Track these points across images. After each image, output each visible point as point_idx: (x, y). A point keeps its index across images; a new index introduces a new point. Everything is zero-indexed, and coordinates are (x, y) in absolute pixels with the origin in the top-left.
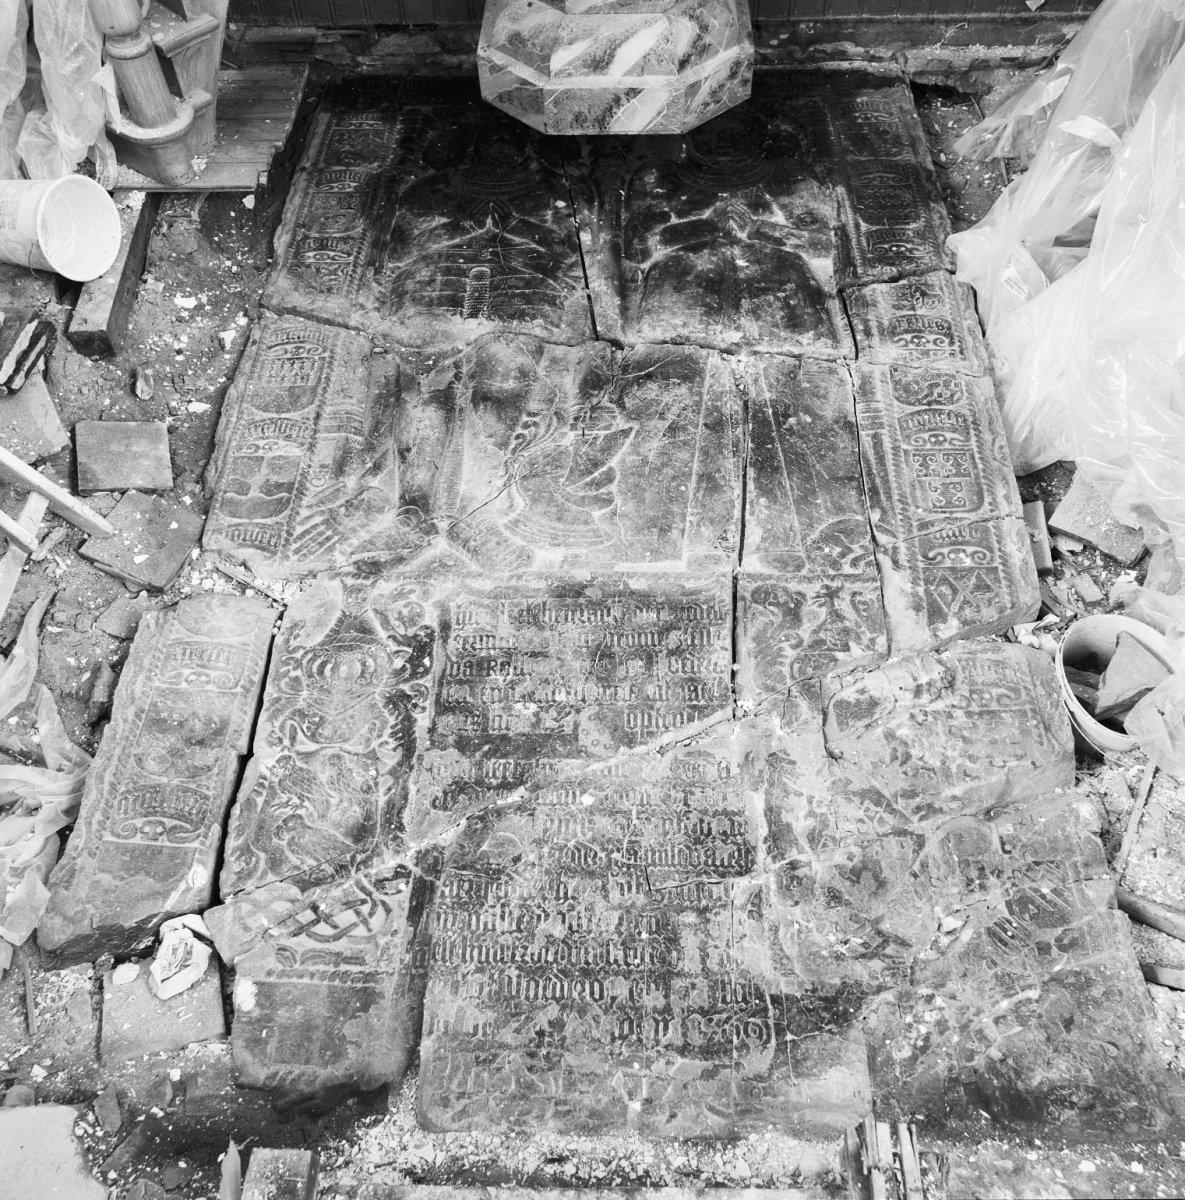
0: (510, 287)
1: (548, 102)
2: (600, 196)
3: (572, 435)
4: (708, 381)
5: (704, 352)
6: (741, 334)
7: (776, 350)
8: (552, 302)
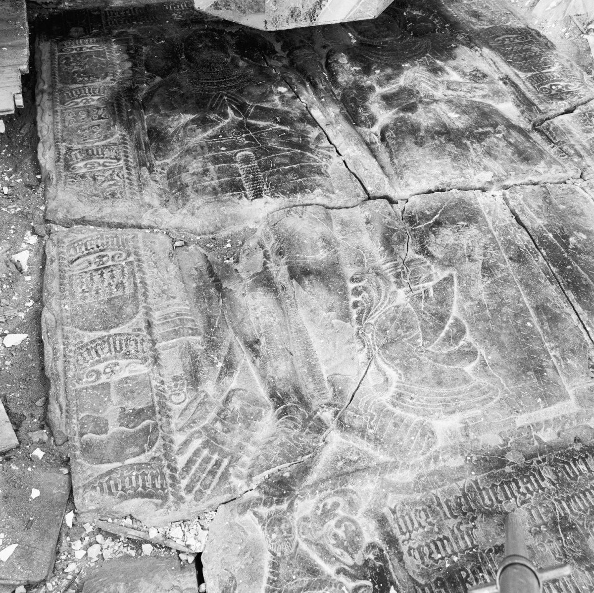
3: (401, 292)
4: (489, 219)
5: (470, 194)
7: (520, 182)
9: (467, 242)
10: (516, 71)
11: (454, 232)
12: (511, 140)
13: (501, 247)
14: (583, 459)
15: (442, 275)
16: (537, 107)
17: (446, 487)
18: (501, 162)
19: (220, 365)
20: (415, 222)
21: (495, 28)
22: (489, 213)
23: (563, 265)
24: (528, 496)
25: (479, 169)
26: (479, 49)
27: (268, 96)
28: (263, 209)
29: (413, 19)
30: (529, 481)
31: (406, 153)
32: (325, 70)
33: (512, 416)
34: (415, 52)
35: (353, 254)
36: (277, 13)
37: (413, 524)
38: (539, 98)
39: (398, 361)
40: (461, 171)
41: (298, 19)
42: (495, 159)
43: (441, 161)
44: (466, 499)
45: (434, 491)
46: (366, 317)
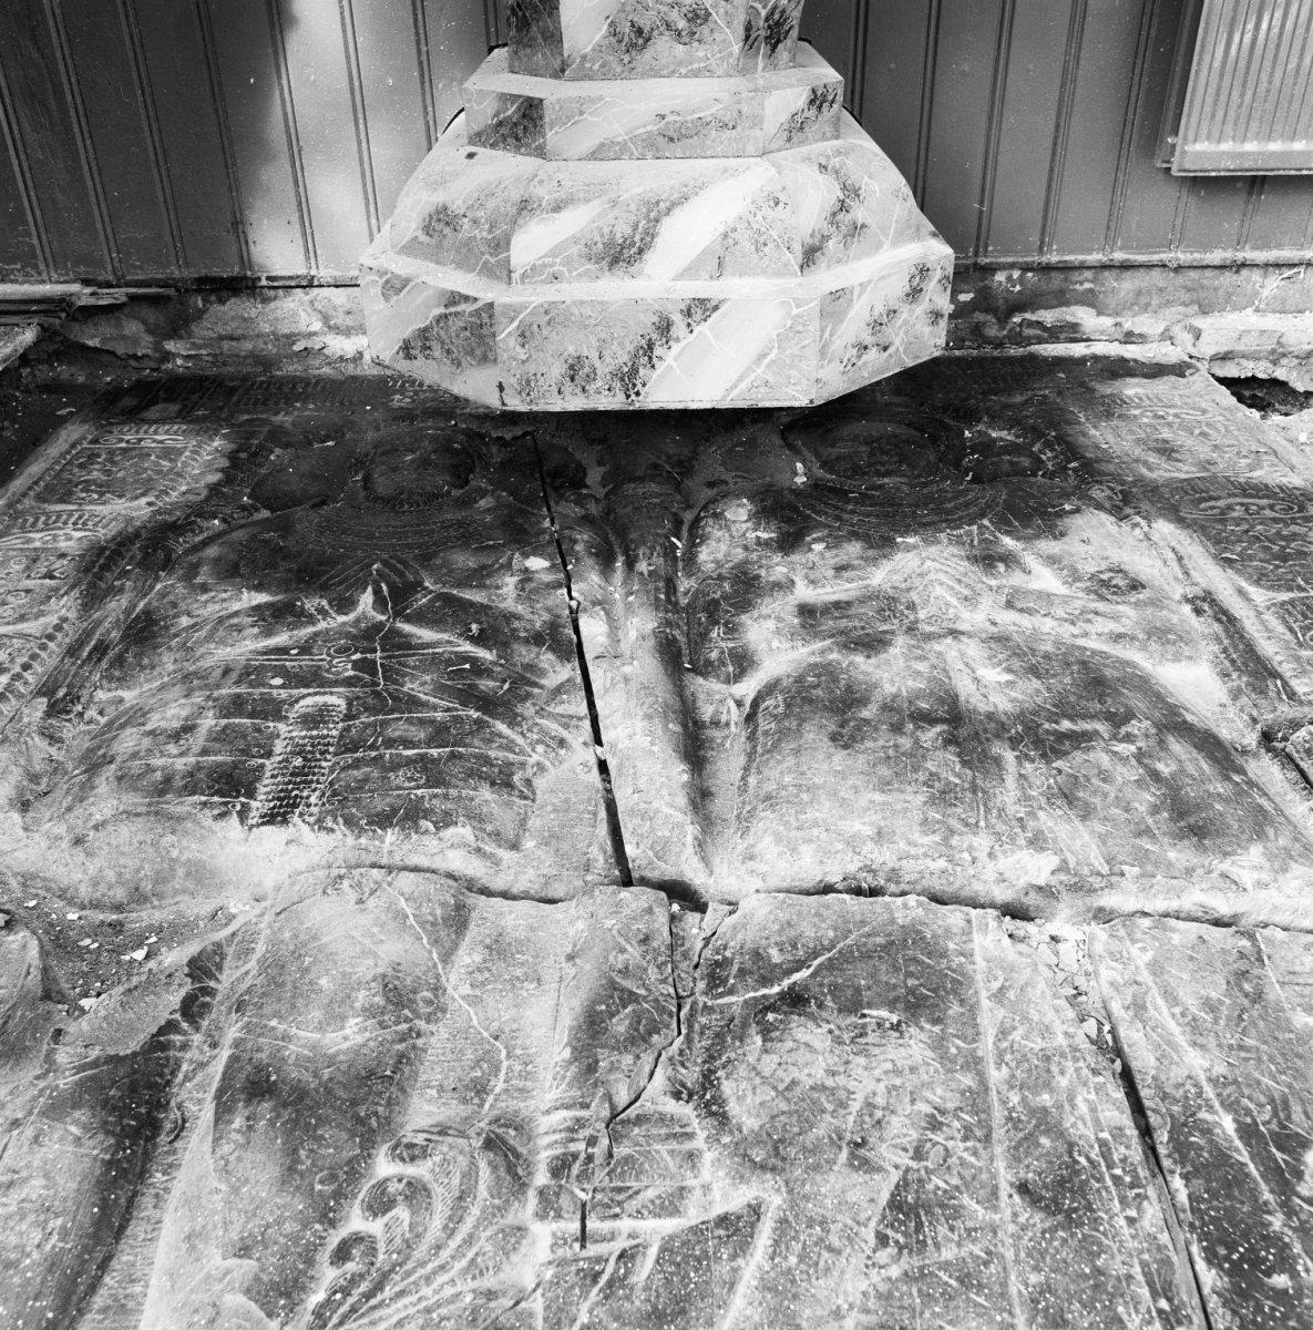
0: (390, 743)
1: (506, 335)
2: (626, 551)
3: (543, 1234)
4: (990, 1017)
5: (953, 916)
6: (1052, 861)
7: (1160, 905)
8: (503, 780)
9: (869, 1085)
10: (1244, 584)
11: (839, 1041)
12: (1160, 767)
13: (999, 1133)
15: (725, 1197)
16: (1285, 684)
18: (1100, 828)
20: (724, 981)
21: (1213, 479)
22: (999, 995)
23: (1256, 1262)
25: (1013, 839)
26: (1143, 523)
27: (490, 575)
28: (277, 861)
29: (986, 447)
31: (791, 761)
32: (685, 534)
34: (949, 512)
35: (470, 1055)
36: (531, 368)
38: (1298, 659)
40: (946, 840)
41: (591, 388)
42: (1084, 818)
43: (889, 798)
46: (353, 1310)
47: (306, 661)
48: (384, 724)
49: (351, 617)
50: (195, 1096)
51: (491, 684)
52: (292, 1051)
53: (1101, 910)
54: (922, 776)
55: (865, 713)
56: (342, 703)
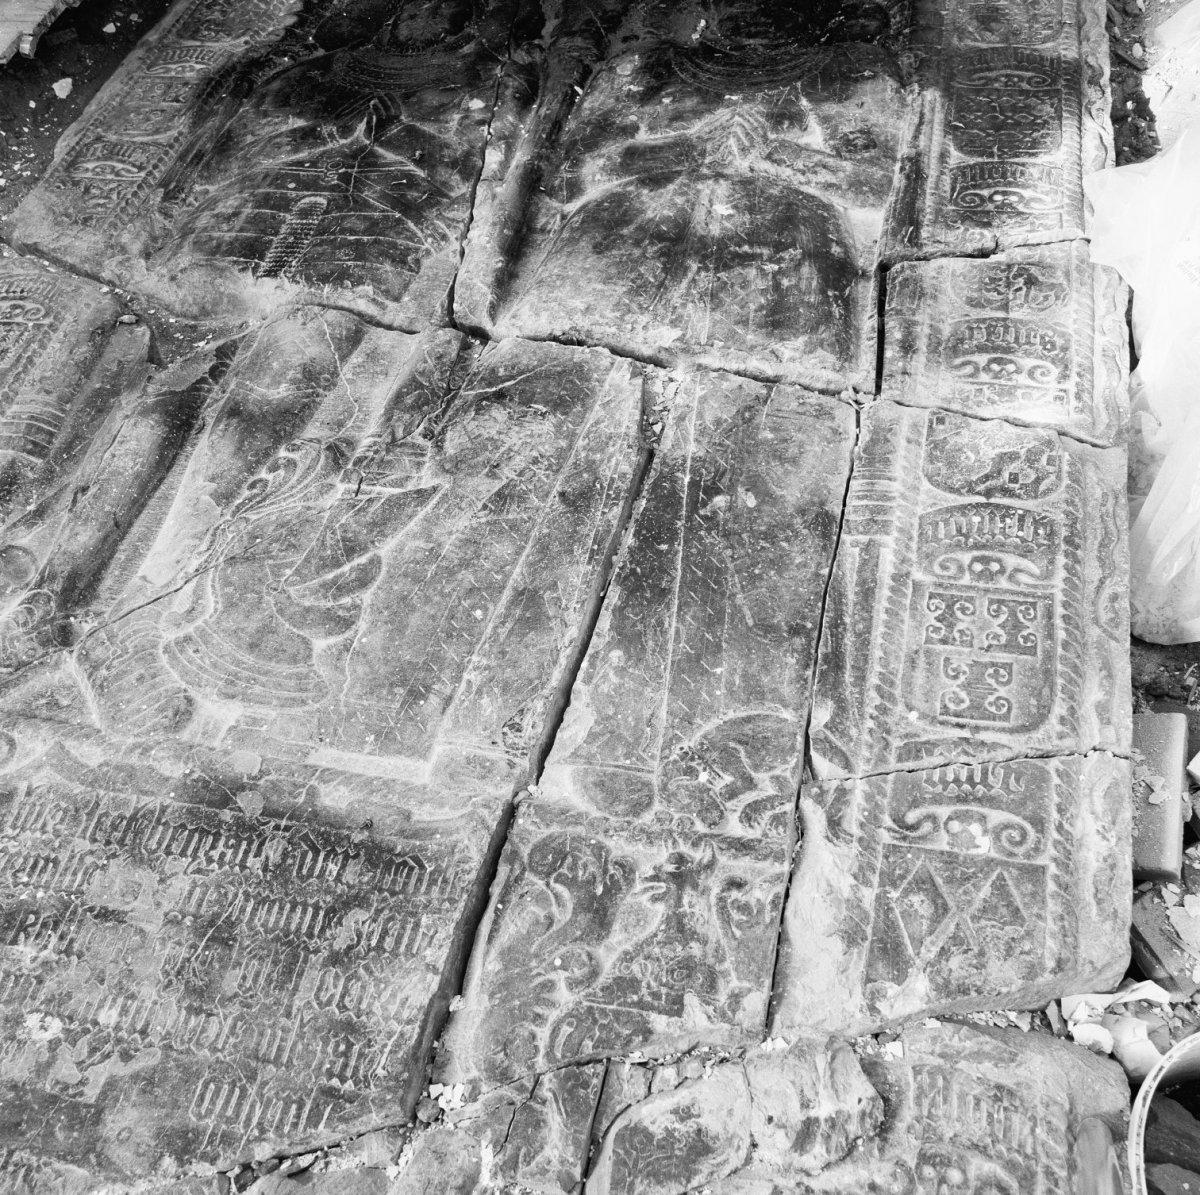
0: (343, 231)
3: (341, 487)
8: (400, 259)
9: (515, 440)
14: (347, 857)
17: (122, 796)
19: (31, 508)
24: (215, 866)
27: (444, 112)
30: (236, 847)
33: (310, 743)
35: (341, 409)
37: (36, 821)
39: (230, 590)
44: (129, 825)
45: (102, 792)
47: (312, 172)
48: (343, 218)
49: (349, 140)
50: (209, 414)
51: (416, 194)
52: (253, 396)
53: (700, 365)
54: (632, 276)
55: (625, 231)
56: (325, 202)
